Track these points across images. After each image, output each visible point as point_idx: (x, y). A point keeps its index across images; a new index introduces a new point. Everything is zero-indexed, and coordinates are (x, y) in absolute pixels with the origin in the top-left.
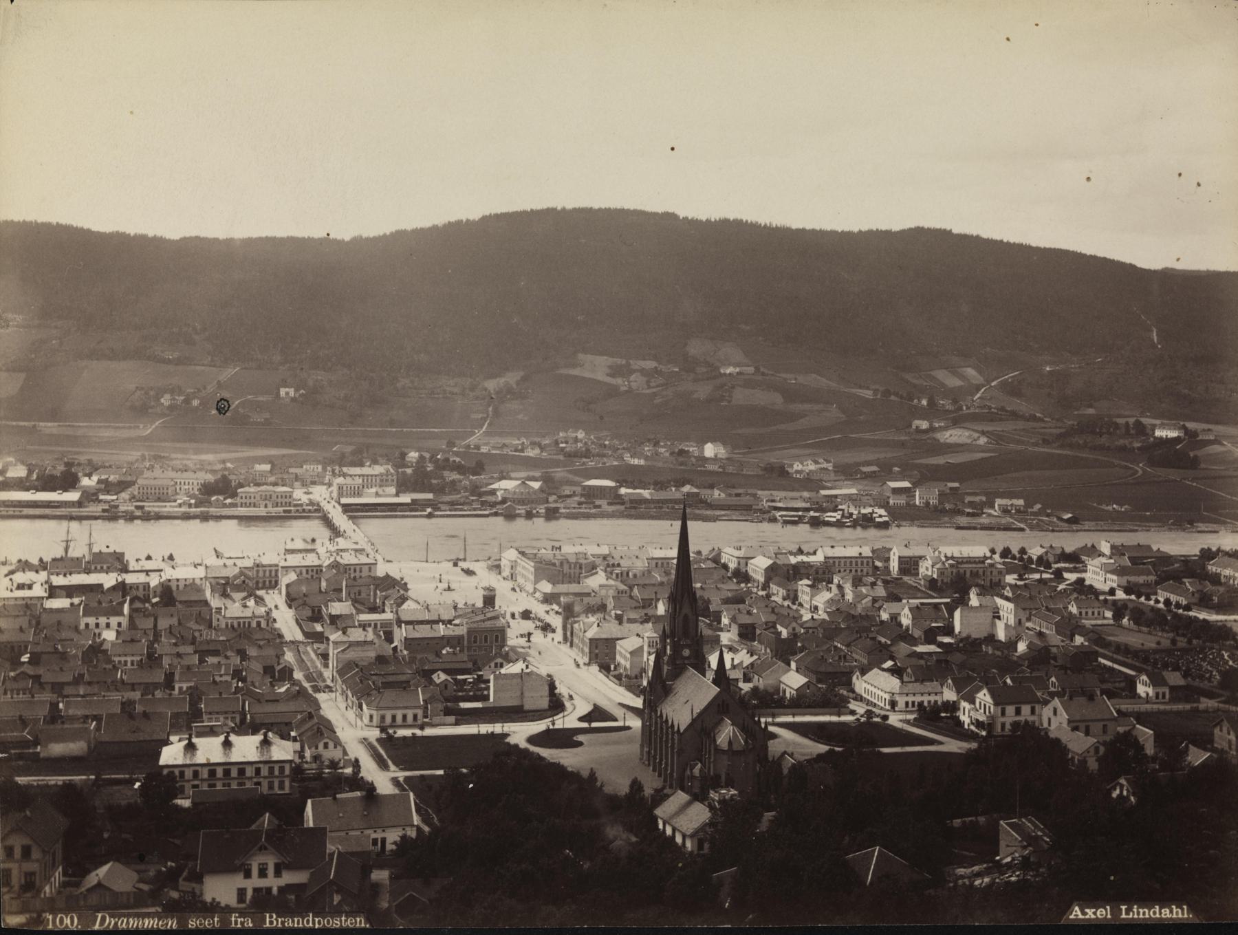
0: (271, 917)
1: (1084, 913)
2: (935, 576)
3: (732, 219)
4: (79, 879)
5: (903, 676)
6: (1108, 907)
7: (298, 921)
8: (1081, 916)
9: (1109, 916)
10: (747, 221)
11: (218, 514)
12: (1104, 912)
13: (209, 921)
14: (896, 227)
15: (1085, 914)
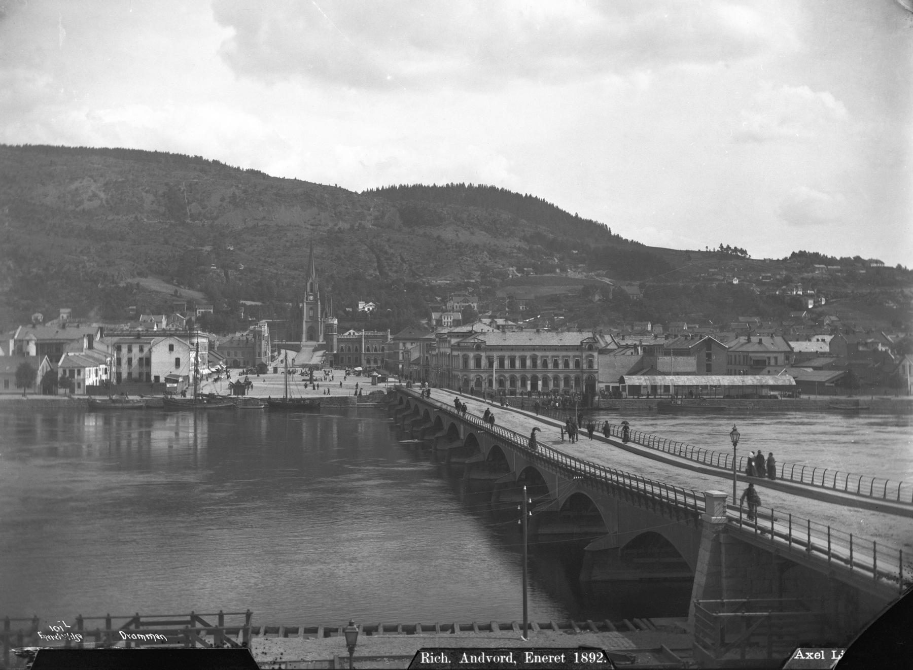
0: (425, 655)
1: (805, 656)
2: (104, 377)
3: (624, 238)
4: (614, 628)
5: (438, 478)
6: (823, 652)
7: (474, 658)
8: (803, 658)
9: (823, 658)
10: (378, 189)
11: (882, 427)
12: (819, 655)
13: (545, 657)
14: (648, 243)
15: (805, 656)
